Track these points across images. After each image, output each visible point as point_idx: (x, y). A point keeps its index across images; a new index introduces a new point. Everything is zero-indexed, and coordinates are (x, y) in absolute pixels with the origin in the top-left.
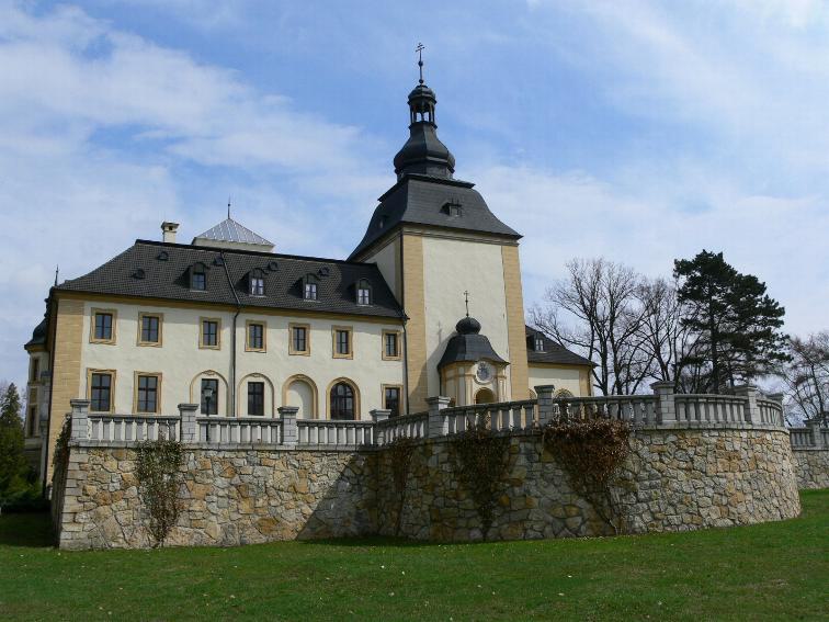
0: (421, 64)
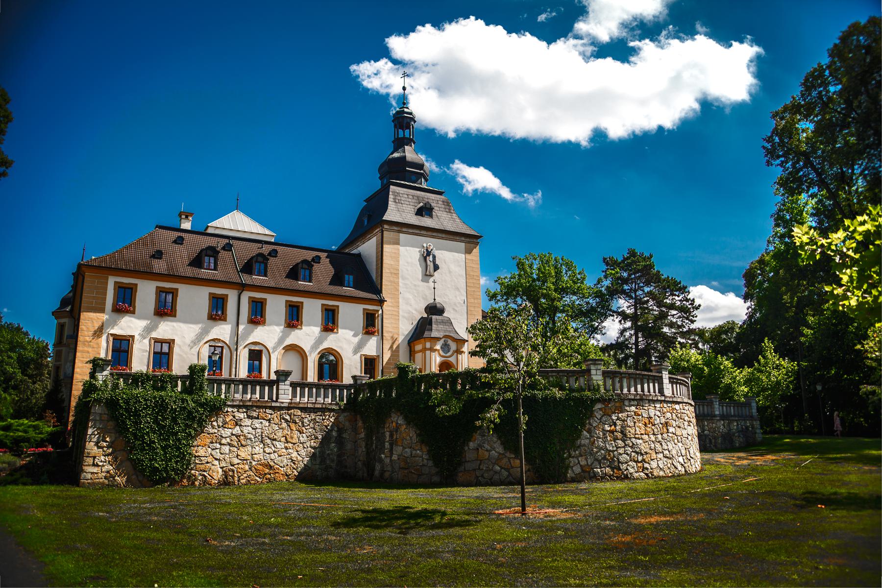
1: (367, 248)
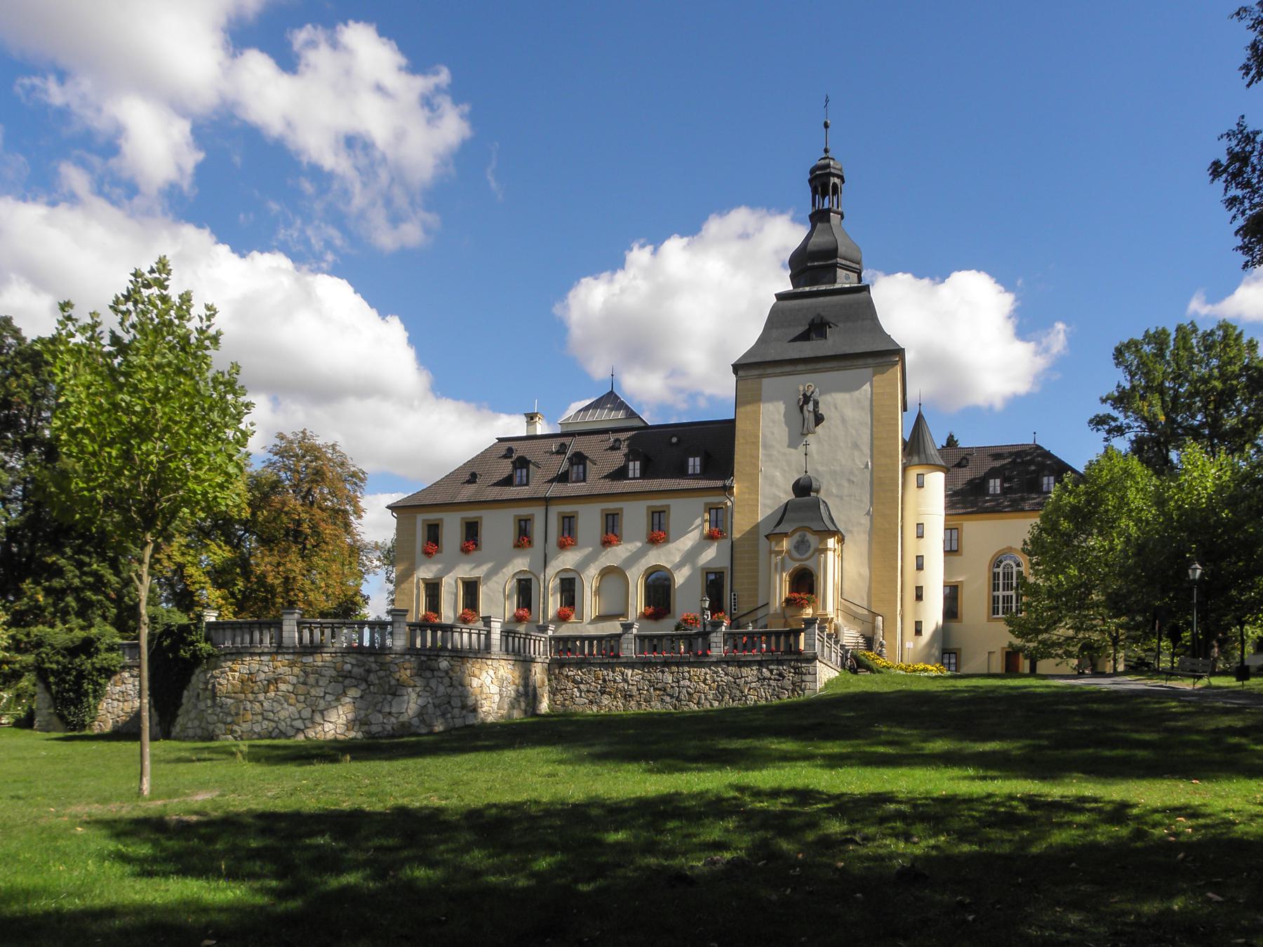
0: (826, 125)
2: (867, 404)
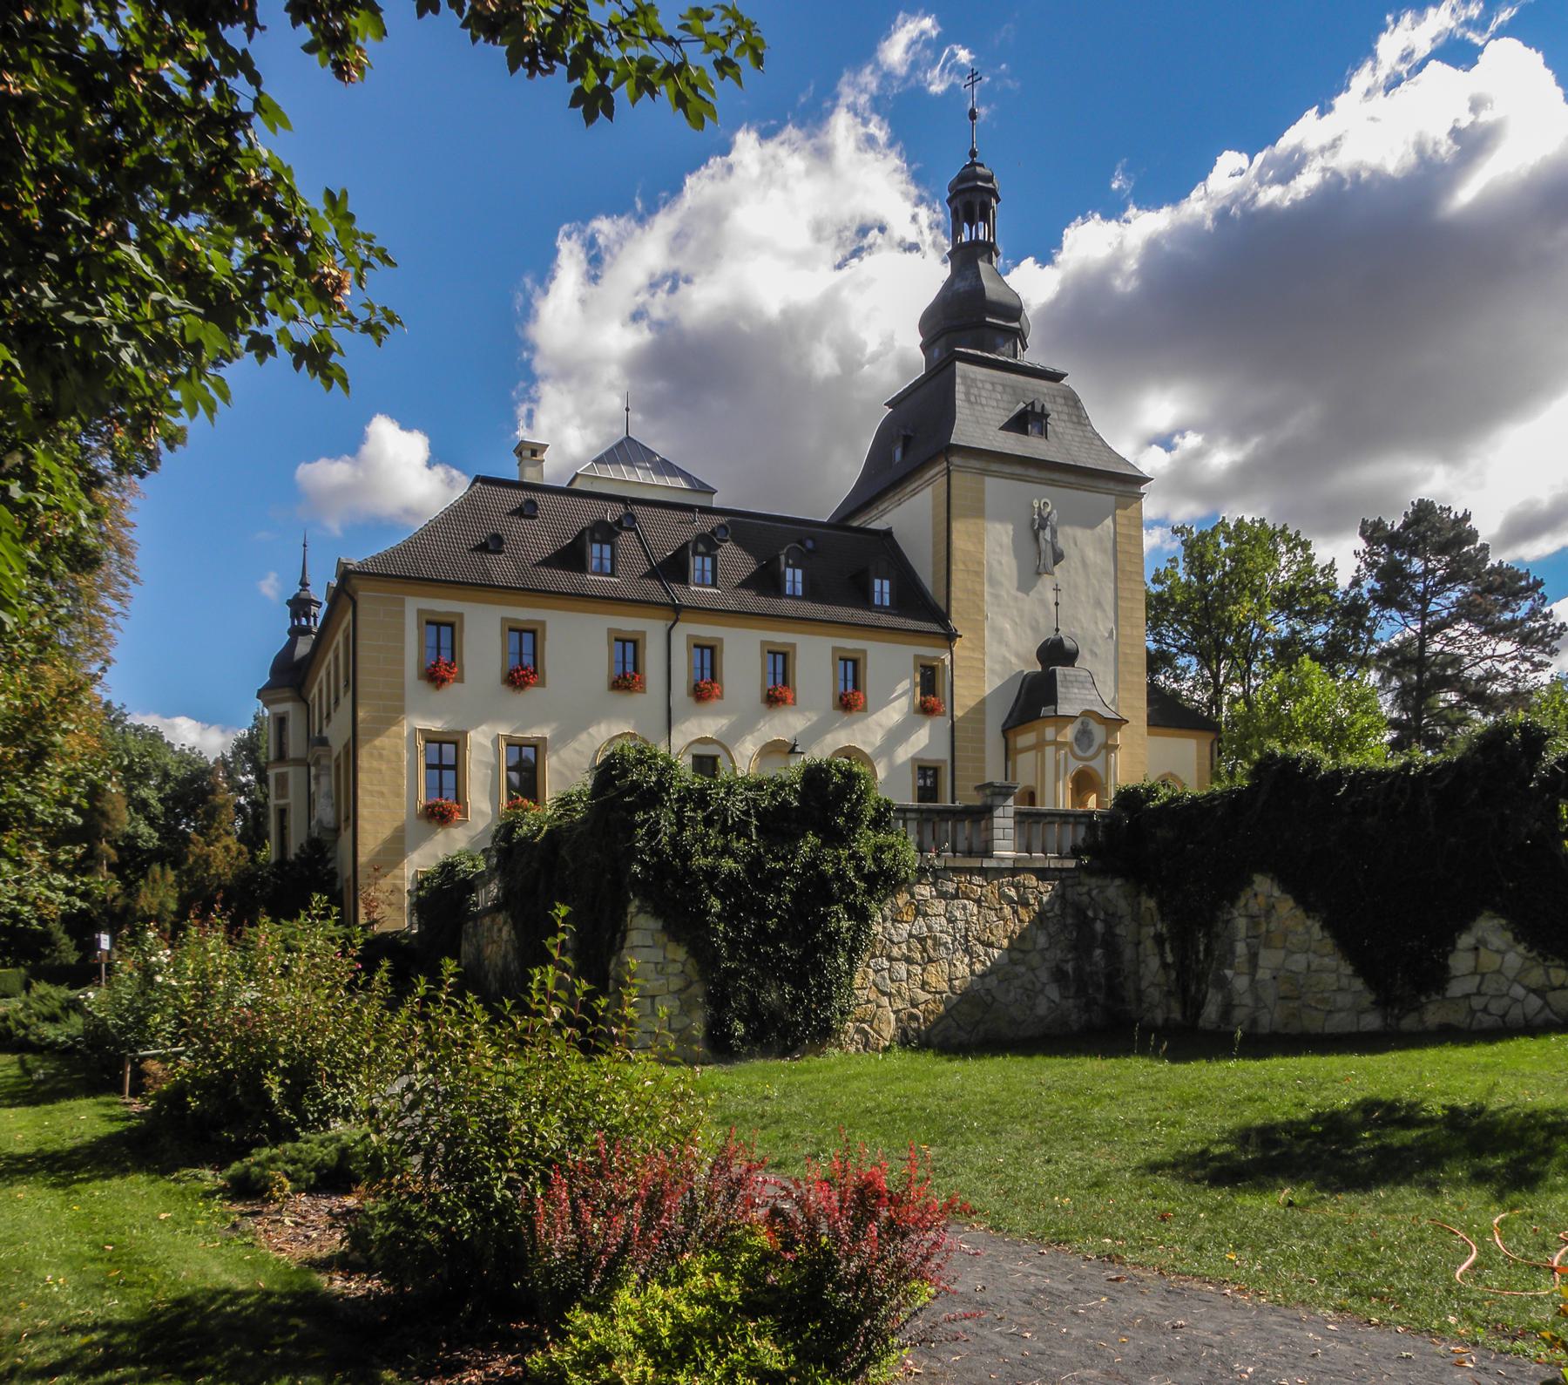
1: (908, 517)
2: (1110, 545)
